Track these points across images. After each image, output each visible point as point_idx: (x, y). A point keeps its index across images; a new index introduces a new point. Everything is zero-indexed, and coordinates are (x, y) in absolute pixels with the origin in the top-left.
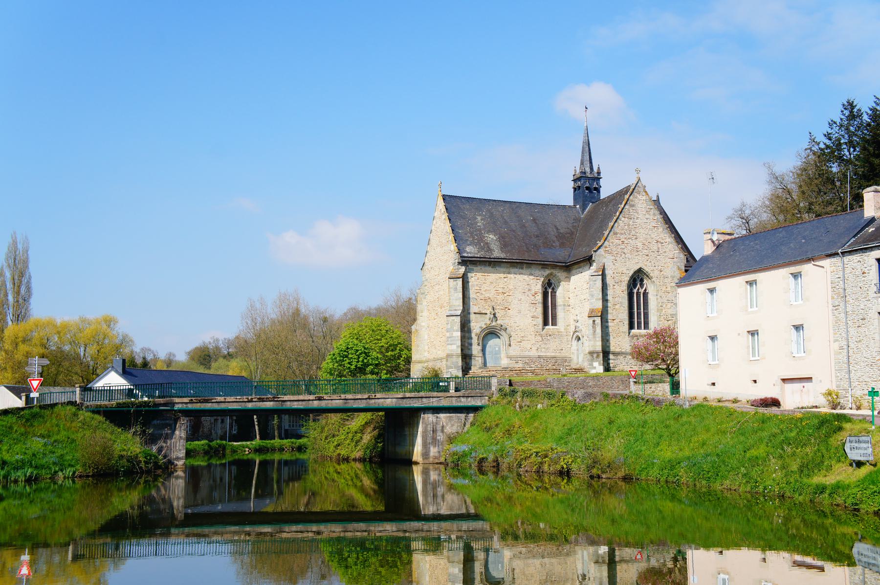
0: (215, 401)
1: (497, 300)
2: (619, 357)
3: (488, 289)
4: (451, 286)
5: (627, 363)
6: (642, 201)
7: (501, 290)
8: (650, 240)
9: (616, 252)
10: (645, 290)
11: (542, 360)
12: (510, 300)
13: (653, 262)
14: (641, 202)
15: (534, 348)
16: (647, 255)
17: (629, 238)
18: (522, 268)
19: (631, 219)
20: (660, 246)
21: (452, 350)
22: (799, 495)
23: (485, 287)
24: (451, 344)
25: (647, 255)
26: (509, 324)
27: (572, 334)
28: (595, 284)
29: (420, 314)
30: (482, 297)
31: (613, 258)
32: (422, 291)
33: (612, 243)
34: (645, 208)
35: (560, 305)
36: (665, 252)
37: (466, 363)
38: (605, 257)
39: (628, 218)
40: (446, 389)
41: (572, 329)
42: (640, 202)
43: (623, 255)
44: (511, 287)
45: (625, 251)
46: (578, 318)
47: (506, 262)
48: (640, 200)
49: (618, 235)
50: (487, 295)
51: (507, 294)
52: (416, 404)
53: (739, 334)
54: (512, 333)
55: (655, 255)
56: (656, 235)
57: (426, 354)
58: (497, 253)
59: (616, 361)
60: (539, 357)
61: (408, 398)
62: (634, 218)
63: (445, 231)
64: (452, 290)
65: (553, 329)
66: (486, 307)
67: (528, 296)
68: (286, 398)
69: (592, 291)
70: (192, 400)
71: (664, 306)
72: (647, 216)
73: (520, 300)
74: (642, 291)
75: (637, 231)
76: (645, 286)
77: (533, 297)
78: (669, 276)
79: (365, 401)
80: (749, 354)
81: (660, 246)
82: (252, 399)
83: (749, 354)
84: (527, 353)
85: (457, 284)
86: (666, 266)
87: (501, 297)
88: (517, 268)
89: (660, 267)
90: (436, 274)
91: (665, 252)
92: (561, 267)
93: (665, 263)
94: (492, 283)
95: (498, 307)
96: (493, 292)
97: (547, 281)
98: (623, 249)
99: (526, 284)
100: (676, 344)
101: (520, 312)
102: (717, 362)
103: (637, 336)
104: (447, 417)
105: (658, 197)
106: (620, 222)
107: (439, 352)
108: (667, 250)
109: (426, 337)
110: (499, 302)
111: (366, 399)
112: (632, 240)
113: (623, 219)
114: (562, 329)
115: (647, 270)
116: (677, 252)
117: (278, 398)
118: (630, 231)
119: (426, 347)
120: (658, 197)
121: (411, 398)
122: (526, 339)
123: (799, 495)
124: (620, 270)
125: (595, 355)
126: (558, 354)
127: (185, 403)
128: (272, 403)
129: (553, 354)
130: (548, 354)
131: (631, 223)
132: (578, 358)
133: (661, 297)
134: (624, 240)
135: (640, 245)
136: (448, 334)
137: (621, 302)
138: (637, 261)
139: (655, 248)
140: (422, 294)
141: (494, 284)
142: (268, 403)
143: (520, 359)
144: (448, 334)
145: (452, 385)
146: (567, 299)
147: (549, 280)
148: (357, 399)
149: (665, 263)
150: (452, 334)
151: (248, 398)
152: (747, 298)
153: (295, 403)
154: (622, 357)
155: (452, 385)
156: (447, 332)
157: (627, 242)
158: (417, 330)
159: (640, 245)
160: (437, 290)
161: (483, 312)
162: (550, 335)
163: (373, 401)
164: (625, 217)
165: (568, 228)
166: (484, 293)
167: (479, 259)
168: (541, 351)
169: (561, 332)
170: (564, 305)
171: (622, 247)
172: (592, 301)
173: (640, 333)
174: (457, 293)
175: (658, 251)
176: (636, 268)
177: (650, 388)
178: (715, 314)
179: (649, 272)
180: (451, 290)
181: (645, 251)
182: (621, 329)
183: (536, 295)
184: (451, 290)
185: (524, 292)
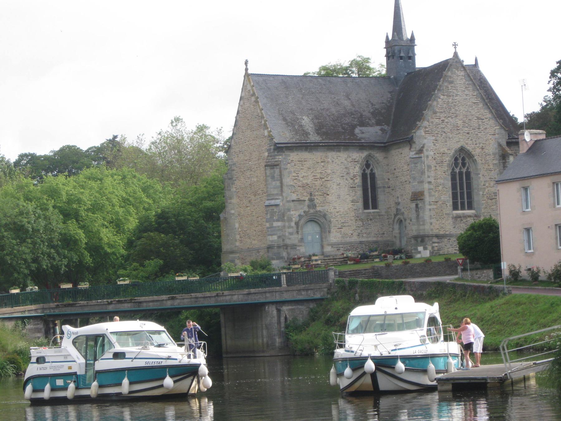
0: (79, 305)
1: (316, 186)
2: (443, 240)
3: (305, 174)
4: (268, 174)
5: (451, 245)
6: (461, 77)
7: (319, 176)
8: (470, 117)
9: (436, 132)
10: (468, 168)
11: (364, 246)
12: (329, 185)
13: (474, 140)
14: (459, 78)
15: (355, 234)
16: (468, 133)
17: (449, 117)
18: (339, 151)
19: (450, 96)
20: (480, 123)
21: (272, 241)
22: (46, 199)
23: (302, 173)
24: (272, 235)
25: (468, 133)
26: (329, 210)
27: (393, 217)
28: (416, 167)
29: (229, 201)
30: (300, 184)
31: (434, 138)
32: (230, 177)
33: (432, 122)
34: (464, 83)
35: (380, 188)
36: (486, 129)
37: (288, 253)
38: (425, 138)
39: (447, 96)
40: (278, 283)
41: (394, 211)
42: (459, 78)
43: (444, 134)
44: (329, 171)
45: (446, 130)
46: (400, 200)
47: (322, 146)
48: (458, 76)
49: (438, 114)
50: (305, 182)
51: (326, 179)
52: (262, 300)
53: (549, 227)
54: (332, 220)
55: (476, 133)
56: (476, 111)
57: (238, 244)
58: (314, 138)
59: (440, 244)
60: (361, 243)
61: (253, 293)
62: (453, 96)
63: (255, 114)
64: (269, 179)
65: (373, 212)
66: (305, 194)
67: (346, 179)
68: (142, 299)
69: (413, 174)
70: (58, 305)
71: (487, 185)
72: (467, 92)
73: (339, 184)
74: (464, 170)
75: (457, 109)
76: (467, 165)
77: (352, 181)
78: (491, 153)
79: (213, 299)
80: (557, 244)
81: (480, 123)
82: (111, 301)
83: (557, 244)
84: (348, 240)
85: (274, 172)
86: (487, 143)
87: (318, 183)
88: (334, 151)
89: (481, 145)
90: (246, 158)
91: (486, 129)
92: (379, 148)
93: (486, 141)
94: (309, 168)
95: (317, 194)
96: (311, 178)
97: (365, 163)
98: (444, 128)
99: (344, 167)
100: (498, 228)
101: (339, 197)
102: (532, 251)
103: (460, 217)
104: (290, 309)
105: (476, 60)
106: (439, 100)
107: (253, 242)
108: (488, 126)
109: (237, 225)
110: (317, 187)
111: (215, 296)
112: (452, 118)
113: (442, 97)
114: (383, 213)
115: (468, 148)
116: (498, 127)
117: (135, 299)
118: (450, 109)
119: (238, 237)
120: (476, 60)
121: (255, 293)
122: (347, 224)
123: (46, 199)
124: (442, 150)
125: (419, 240)
126: (380, 239)
127: (52, 308)
128: (129, 305)
129: (375, 239)
130: (370, 239)
131: (450, 100)
132: (401, 241)
133: (483, 175)
134: (443, 119)
135: (460, 123)
136: (268, 225)
137: (443, 183)
138: (458, 140)
139: (476, 125)
140: (230, 179)
141: (312, 170)
142: (126, 305)
143: (342, 246)
144: (268, 225)
145: (284, 278)
146: (387, 180)
147: (367, 161)
148: (207, 297)
149: (486, 141)
150: (272, 224)
151: (108, 301)
152: (554, 197)
153: (151, 304)
154: (446, 240)
155: (284, 278)
156: (267, 222)
157: (446, 121)
158: (226, 219)
159: (460, 123)
160: (249, 176)
161: (302, 199)
162: (371, 220)
163: (221, 298)
164: (444, 95)
165: (383, 103)
166: (301, 179)
167: (295, 145)
168: (363, 236)
169: (382, 215)
170: (384, 187)
171: (442, 126)
172: (414, 184)
173: (463, 214)
174: (274, 181)
175: (479, 128)
176: (458, 146)
177: (477, 274)
178: (529, 210)
179: (471, 150)
180: (268, 178)
181: (466, 129)
182: (444, 210)
183: (355, 179)
184: (268, 178)
185: (342, 176)
